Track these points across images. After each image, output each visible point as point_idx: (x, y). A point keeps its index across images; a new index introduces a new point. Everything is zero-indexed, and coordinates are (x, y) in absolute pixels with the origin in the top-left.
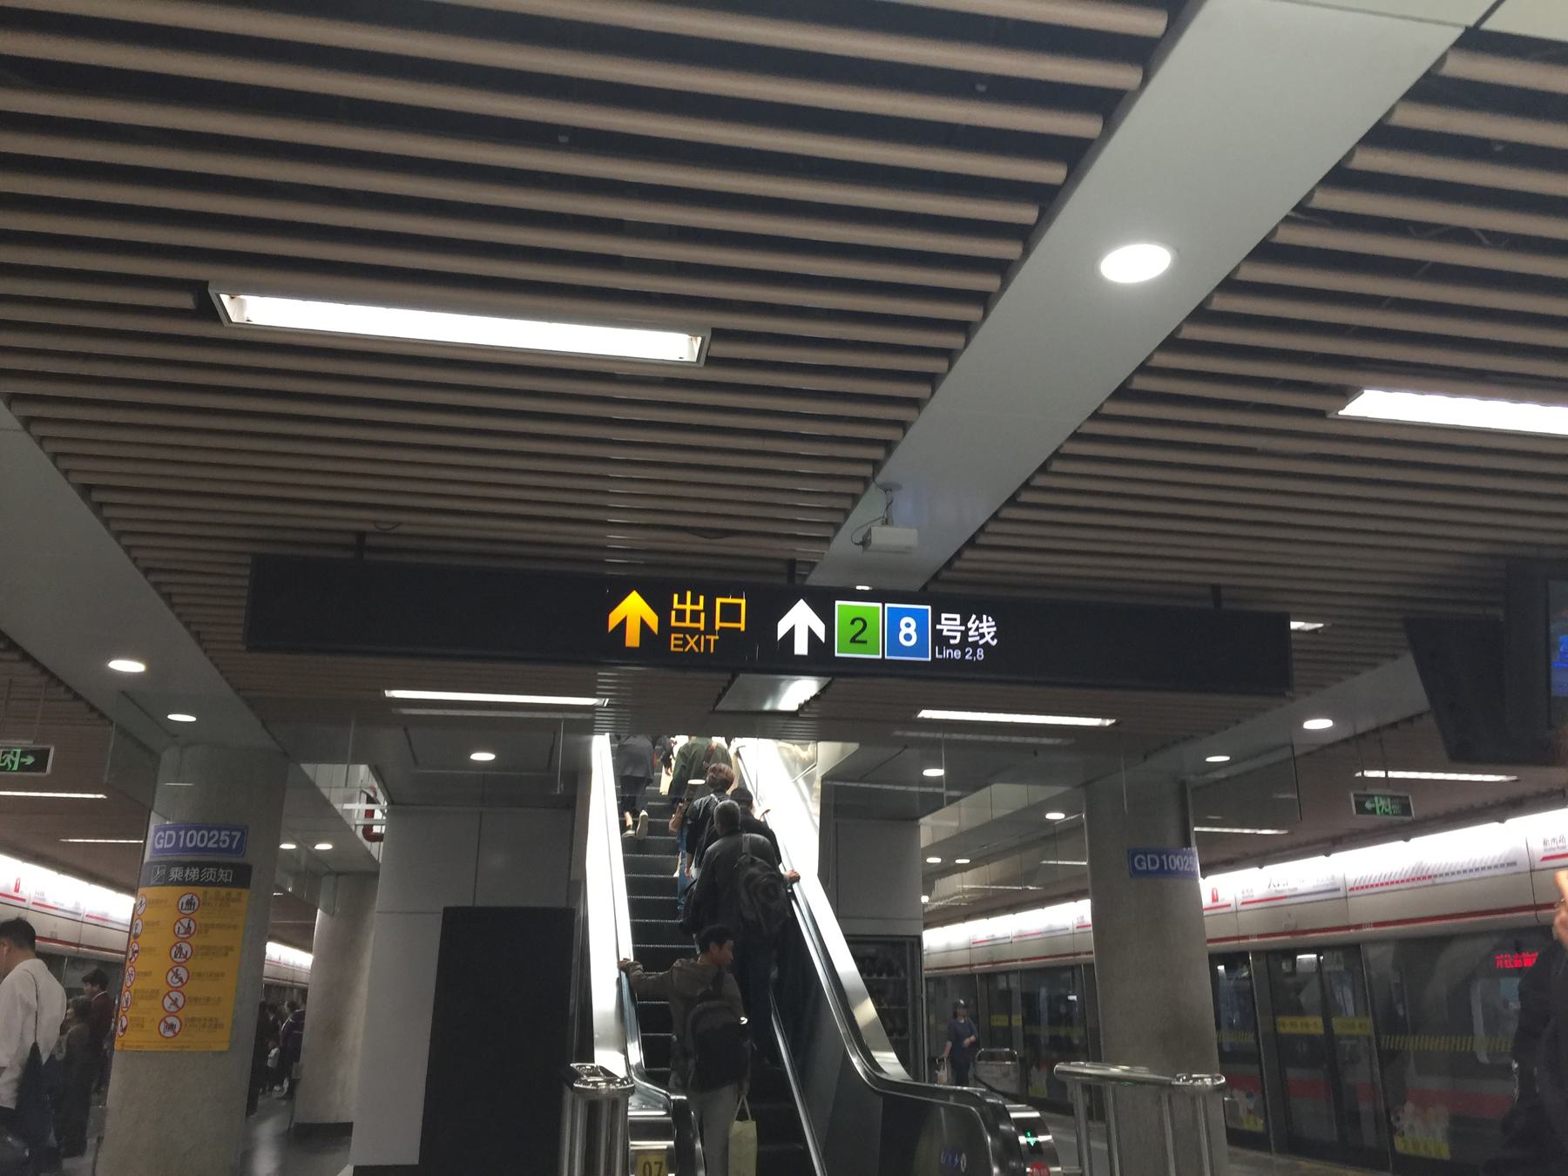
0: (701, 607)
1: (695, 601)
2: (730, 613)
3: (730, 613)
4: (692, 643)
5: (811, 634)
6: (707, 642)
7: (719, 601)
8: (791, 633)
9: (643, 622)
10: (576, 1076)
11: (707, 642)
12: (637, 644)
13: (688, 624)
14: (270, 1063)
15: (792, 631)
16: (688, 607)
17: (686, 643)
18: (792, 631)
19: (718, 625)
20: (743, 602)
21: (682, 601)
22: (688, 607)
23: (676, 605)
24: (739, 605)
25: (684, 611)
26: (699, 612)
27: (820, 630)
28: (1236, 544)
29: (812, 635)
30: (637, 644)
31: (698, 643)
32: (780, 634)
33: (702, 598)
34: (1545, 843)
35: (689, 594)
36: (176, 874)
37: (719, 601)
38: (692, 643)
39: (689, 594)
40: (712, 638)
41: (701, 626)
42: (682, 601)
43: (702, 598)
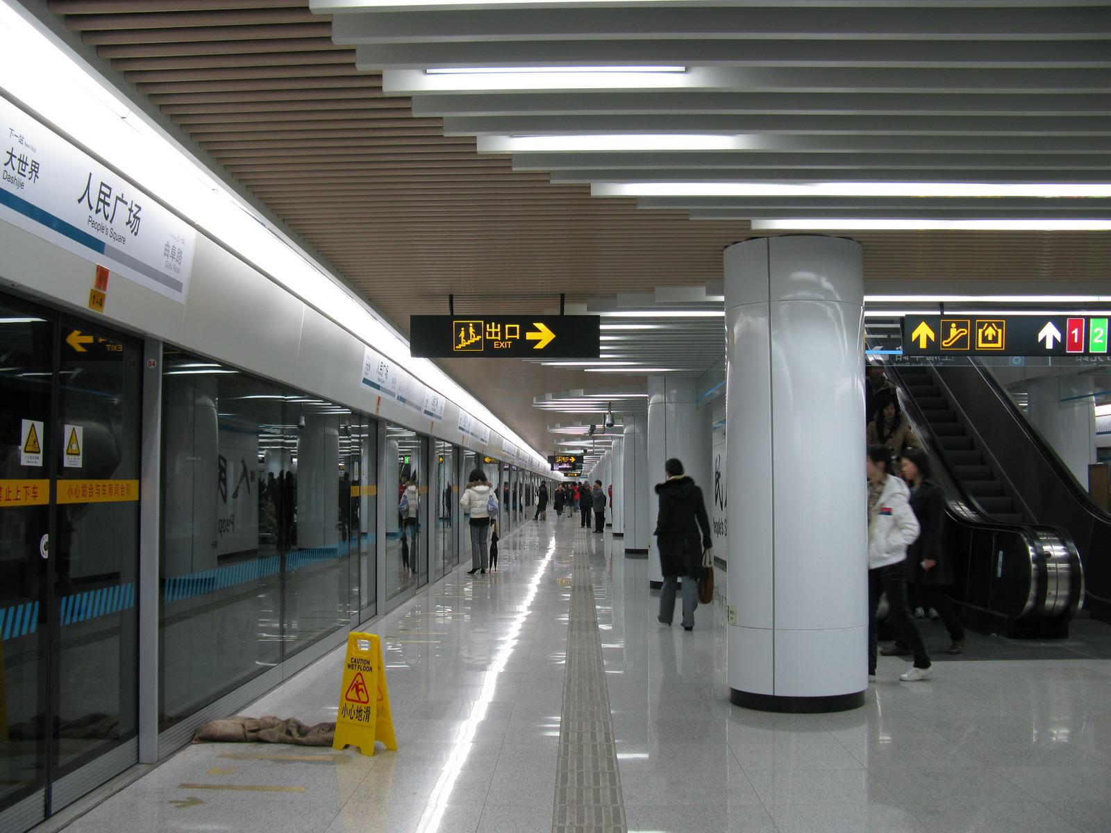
0: (499, 330)
1: (496, 327)
2: (512, 331)
3: (512, 331)
4: (502, 345)
5: (928, 338)
6: (508, 344)
7: (507, 326)
8: (918, 338)
9: (927, 336)
10: (1052, 735)
11: (508, 344)
12: (925, 347)
13: (493, 337)
14: (303, 418)
15: (919, 337)
16: (493, 330)
17: (500, 345)
18: (919, 337)
19: (507, 337)
20: (518, 326)
21: (491, 327)
22: (493, 330)
23: (488, 330)
24: (516, 328)
25: (491, 332)
26: (498, 332)
27: (1059, 337)
28: (669, 223)
29: (1055, 339)
30: (925, 347)
31: (504, 345)
32: (1040, 339)
33: (499, 326)
34: (243, 726)
35: (493, 324)
36: (436, 401)
37: (507, 326)
38: (502, 345)
39: (493, 324)
40: (509, 343)
41: (499, 338)
42: (491, 327)
43: (499, 326)
